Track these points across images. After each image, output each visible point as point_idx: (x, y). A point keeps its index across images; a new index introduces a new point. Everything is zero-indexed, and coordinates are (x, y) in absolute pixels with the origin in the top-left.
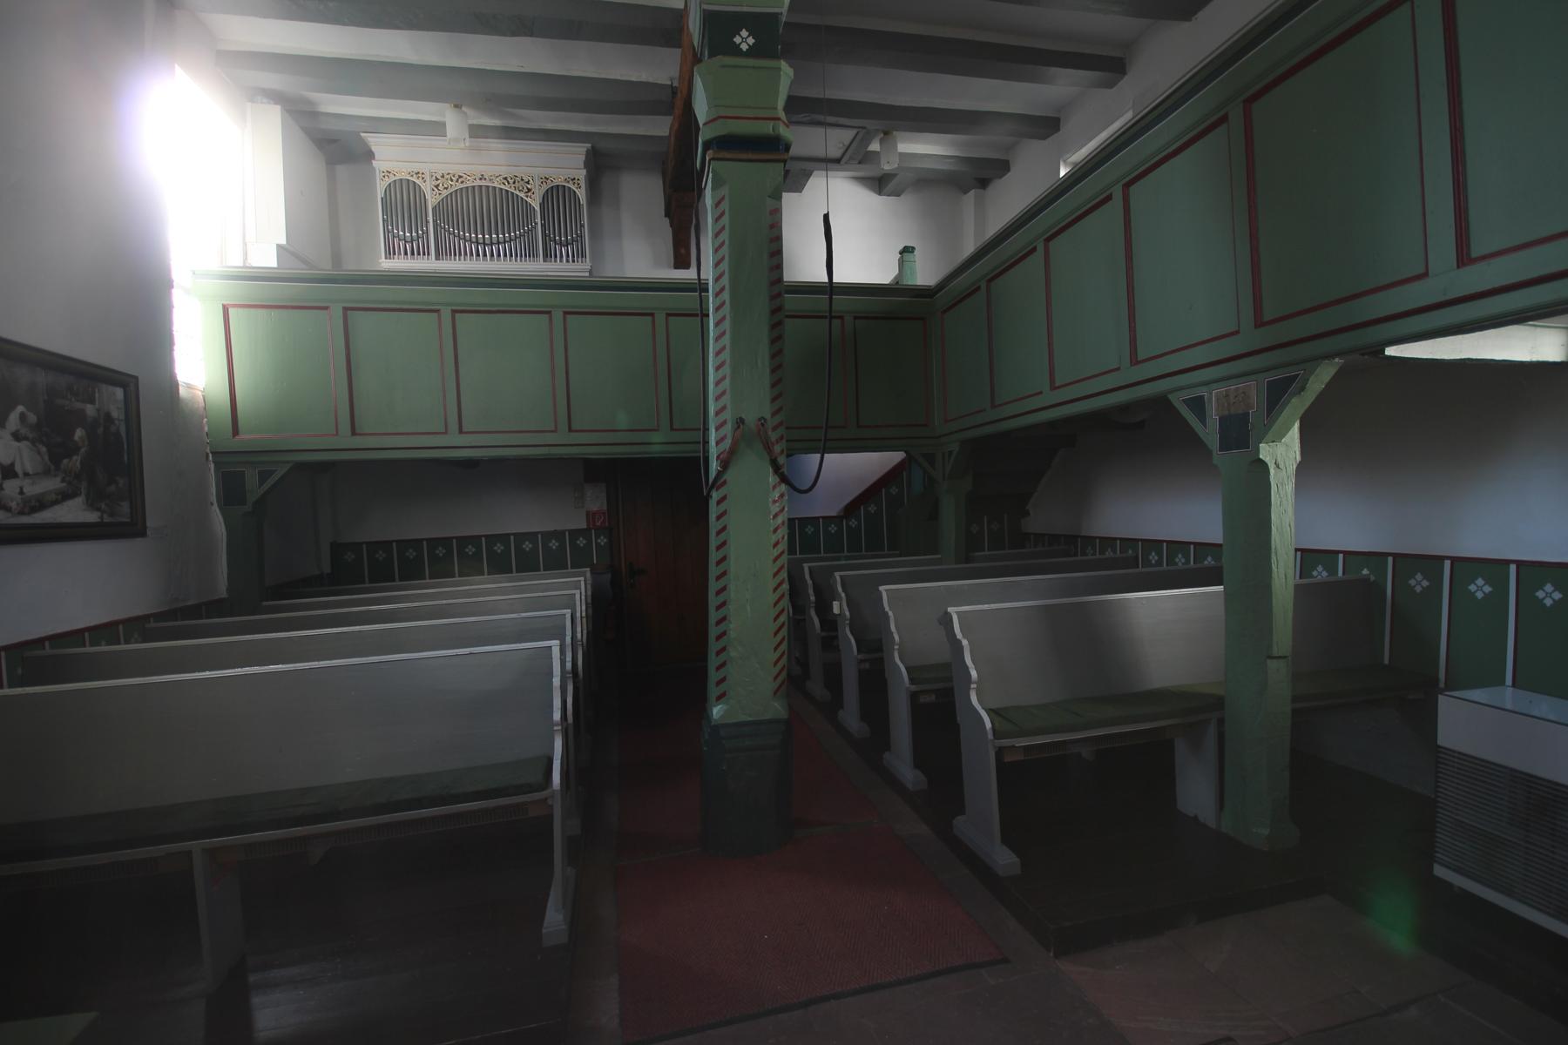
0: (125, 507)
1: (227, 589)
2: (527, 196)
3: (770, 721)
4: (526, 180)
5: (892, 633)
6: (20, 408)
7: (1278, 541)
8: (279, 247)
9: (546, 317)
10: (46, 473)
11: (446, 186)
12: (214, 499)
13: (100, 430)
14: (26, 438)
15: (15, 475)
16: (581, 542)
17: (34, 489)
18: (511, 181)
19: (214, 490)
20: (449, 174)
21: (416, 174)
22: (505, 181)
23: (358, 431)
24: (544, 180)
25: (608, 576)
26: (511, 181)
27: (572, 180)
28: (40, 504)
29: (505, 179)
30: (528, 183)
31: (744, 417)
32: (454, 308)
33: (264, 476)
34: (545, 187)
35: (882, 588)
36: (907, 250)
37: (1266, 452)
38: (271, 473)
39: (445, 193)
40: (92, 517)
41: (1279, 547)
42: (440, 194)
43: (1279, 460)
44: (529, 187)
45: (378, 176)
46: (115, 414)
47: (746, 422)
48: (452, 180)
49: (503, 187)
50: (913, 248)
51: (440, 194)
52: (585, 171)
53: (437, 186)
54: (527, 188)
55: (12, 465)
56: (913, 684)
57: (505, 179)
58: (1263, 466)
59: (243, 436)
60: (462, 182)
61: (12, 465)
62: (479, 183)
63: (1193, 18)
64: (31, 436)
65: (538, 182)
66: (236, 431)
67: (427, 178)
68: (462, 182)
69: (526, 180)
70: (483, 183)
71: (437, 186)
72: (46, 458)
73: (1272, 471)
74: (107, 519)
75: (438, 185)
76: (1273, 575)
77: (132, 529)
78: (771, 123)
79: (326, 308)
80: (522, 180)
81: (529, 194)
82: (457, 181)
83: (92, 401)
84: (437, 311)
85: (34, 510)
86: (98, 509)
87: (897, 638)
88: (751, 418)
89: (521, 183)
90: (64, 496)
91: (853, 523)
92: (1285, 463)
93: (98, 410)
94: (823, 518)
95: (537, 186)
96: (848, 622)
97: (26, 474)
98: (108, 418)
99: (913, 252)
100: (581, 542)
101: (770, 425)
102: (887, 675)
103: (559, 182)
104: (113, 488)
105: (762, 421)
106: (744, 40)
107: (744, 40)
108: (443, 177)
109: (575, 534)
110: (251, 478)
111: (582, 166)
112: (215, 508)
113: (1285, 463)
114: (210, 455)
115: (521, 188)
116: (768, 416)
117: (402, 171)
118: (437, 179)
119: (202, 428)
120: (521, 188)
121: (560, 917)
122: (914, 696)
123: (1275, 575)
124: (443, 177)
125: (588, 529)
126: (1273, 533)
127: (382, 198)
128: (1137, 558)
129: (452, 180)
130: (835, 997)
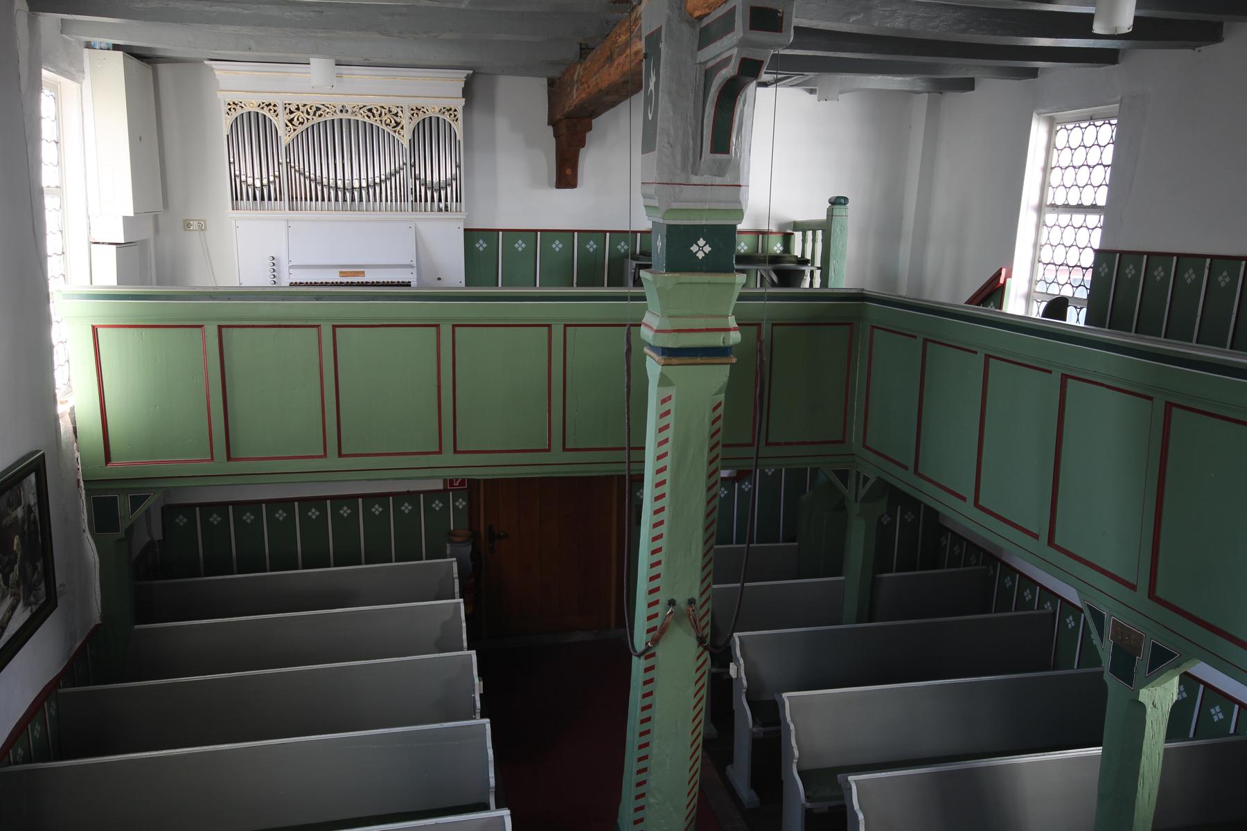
1: (101, 616)
2: (395, 131)
4: (394, 111)
5: (793, 748)
7: (1146, 768)
8: (126, 219)
11: (301, 120)
16: (437, 505)
19: (85, 516)
20: (305, 105)
21: (267, 106)
22: (370, 114)
23: (232, 456)
24: (416, 111)
25: (469, 548)
27: (448, 110)
29: (370, 110)
30: (396, 115)
31: (675, 598)
32: (335, 323)
33: (136, 502)
34: (416, 120)
35: (785, 695)
36: (837, 202)
37: (1145, 695)
39: (300, 128)
41: (373, 102)
42: (295, 130)
43: (1156, 702)
44: (398, 120)
47: (677, 603)
48: (308, 113)
49: (367, 119)
50: (846, 199)
51: (295, 130)
52: (464, 100)
54: (396, 122)
56: (808, 801)
57: (370, 110)
58: (1142, 707)
60: (321, 115)
62: (339, 116)
63: (1197, 49)
65: (408, 114)
66: (108, 458)
67: (280, 109)
68: (321, 115)
69: (394, 111)
70: (345, 116)
71: (291, 121)
73: (1149, 710)
75: (292, 119)
76: (1138, 795)
78: (723, 334)
80: (390, 111)
81: (398, 128)
82: (314, 115)
87: (796, 753)
88: (681, 600)
90: (13, 608)
91: (746, 486)
92: (1161, 704)
95: (407, 118)
96: (745, 690)
99: (845, 204)
100: (437, 505)
101: (698, 603)
102: (783, 778)
103: (433, 112)
105: (691, 602)
106: (701, 249)
107: (701, 249)
108: (298, 109)
109: (430, 495)
110: (124, 504)
111: (461, 96)
112: (88, 535)
113: (1161, 704)
114: (82, 484)
115: (388, 121)
116: (696, 595)
117: (251, 103)
118: (291, 112)
120: (388, 121)
122: (808, 813)
123: (1139, 795)
125: (445, 490)
126: (1142, 760)
127: (228, 136)
128: (1054, 614)
129: (308, 113)
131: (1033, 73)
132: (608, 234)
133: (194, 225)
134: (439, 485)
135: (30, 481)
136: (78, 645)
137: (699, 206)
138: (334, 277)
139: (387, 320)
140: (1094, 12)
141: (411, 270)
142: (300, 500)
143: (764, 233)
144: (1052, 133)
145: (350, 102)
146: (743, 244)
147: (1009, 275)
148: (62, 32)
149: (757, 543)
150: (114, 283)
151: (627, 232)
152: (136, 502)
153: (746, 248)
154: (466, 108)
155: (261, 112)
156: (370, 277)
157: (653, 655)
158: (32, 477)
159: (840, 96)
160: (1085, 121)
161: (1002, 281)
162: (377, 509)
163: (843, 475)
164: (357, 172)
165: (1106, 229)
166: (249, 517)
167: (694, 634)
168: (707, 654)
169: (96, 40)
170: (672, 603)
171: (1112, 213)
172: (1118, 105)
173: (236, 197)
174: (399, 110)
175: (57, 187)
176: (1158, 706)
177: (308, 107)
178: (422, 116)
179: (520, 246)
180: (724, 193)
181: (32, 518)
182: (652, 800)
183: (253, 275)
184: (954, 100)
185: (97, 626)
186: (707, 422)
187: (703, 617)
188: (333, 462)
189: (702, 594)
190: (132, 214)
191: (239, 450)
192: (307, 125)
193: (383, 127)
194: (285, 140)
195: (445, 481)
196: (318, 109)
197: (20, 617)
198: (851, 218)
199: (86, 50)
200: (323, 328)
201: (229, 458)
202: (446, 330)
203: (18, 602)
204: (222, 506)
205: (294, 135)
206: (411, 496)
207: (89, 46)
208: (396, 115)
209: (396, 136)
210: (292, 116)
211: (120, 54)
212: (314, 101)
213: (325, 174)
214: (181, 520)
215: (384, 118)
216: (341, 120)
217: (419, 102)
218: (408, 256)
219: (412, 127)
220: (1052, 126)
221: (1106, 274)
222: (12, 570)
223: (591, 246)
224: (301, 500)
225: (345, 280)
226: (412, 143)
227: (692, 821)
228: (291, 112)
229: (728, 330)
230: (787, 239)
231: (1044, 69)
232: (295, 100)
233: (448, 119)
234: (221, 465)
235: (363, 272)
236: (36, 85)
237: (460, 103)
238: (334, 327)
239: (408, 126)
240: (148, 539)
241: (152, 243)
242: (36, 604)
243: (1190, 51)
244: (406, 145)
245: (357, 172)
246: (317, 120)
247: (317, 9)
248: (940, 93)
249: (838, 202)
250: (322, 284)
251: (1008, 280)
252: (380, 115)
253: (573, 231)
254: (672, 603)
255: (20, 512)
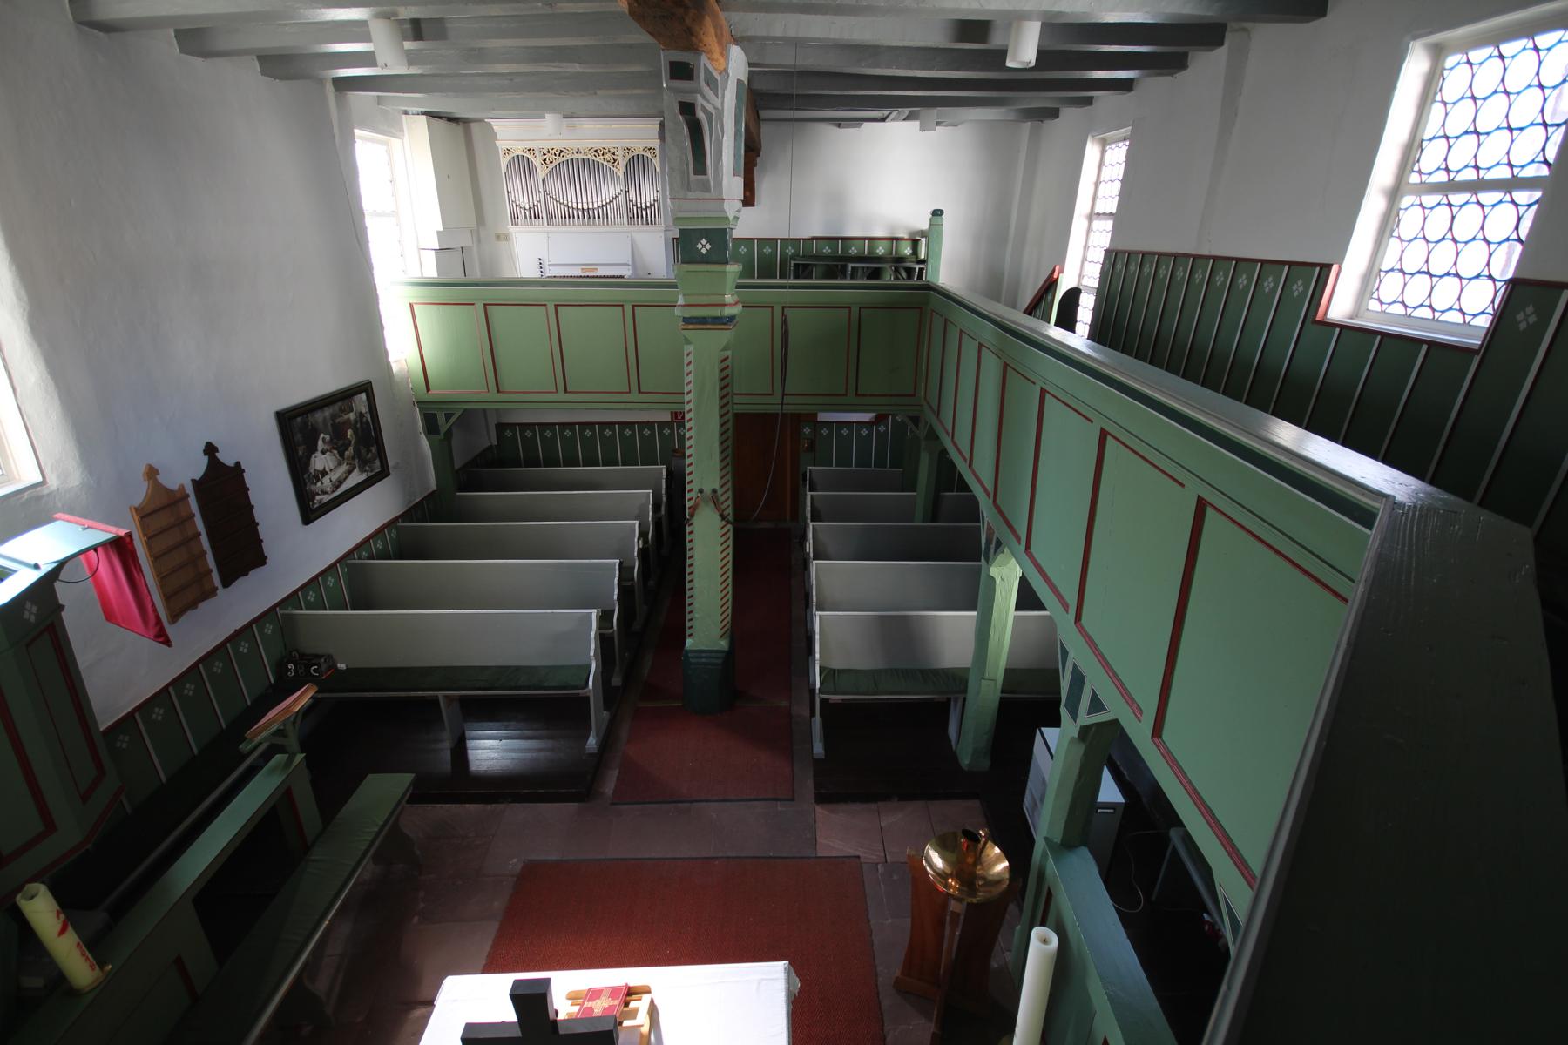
0: (377, 462)
3: (717, 651)
4: (612, 150)
6: (322, 435)
8: (438, 232)
9: (621, 307)
10: (340, 464)
12: (421, 430)
13: (358, 425)
14: (328, 451)
15: (327, 473)
16: (667, 431)
17: (335, 476)
18: (601, 153)
19: (420, 424)
21: (529, 150)
23: (501, 390)
26: (601, 153)
28: (340, 482)
29: (596, 151)
32: (557, 303)
33: (448, 416)
38: (452, 414)
40: (363, 477)
41: (598, 144)
44: (615, 157)
45: (501, 154)
46: (364, 411)
48: (555, 155)
53: (545, 161)
55: (324, 469)
57: (596, 151)
59: (433, 391)
61: (324, 469)
62: (576, 156)
64: (329, 448)
66: (428, 389)
67: (537, 152)
69: (612, 150)
71: (545, 161)
72: (337, 456)
74: (370, 474)
77: (384, 473)
79: (473, 304)
81: (616, 163)
83: (352, 411)
84: (545, 305)
85: (337, 487)
86: (365, 471)
88: (708, 490)
89: (609, 154)
90: (350, 472)
91: (882, 429)
93: (356, 414)
94: (857, 422)
97: (331, 470)
98: (361, 415)
100: (667, 431)
104: (370, 455)
107: (704, 246)
108: (548, 152)
109: (662, 425)
110: (441, 418)
112: (423, 435)
117: (518, 149)
118: (544, 154)
119: (408, 385)
121: (594, 742)
124: (548, 152)
129: (555, 155)
130: (707, 801)
131: (1089, 101)
132: (756, 241)
133: (502, 237)
134: (668, 418)
135: (361, 398)
136: (417, 500)
137: (696, 215)
138: (577, 272)
139: (581, 301)
140: (372, 49)
141: (627, 267)
142: (579, 424)
143: (897, 239)
144: (1103, 152)
145: (583, 145)
146: (880, 248)
147: (1062, 271)
148: (378, 104)
149: (890, 467)
150: (436, 275)
151: (787, 239)
152: (448, 416)
153: (883, 251)
154: (662, 148)
155: (525, 155)
156: (601, 272)
157: (692, 524)
158: (363, 396)
159: (937, 128)
160: (1121, 141)
161: (1055, 276)
162: (628, 432)
163: (915, 420)
164: (590, 198)
165: (1116, 232)
166: (548, 434)
167: (718, 514)
168: (729, 527)
169: (408, 109)
170: (701, 491)
171: (1120, 219)
172: (1130, 128)
173: (515, 217)
174: (615, 150)
175: (393, 212)
176: (1005, 579)
177: (554, 150)
178: (631, 155)
179: (704, 246)
180: (712, 205)
181: (364, 420)
182: (696, 615)
183: (525, 268)
184: (1050, 124)
185: (434, 492)
186: (717, 371)
187: (726, 500)
188: (561, 396)
189: (722, 486)
190: (442, 229)
191: (505, 386)
192: (555, 163)
193: (606, 163)
194: (541, 174)
195: (672, 413)
196: (562, 151)
197: (356, 478)
198: (948, 223)
199: (404, 116)
200: (548, 306)
201: (498, 391)
202: (628, 309)
203: (354, 469)
204: (531, 426)
205: (547, 171)
206: (649, 425)
207: (406, 113)
208: (614, 154)
209: (614, 169)
210: (545, 157)
211: (424, 117)
212: (558, 145)
213: (569, 200)
214: (508, 433)
215: (606, 156)
216: (578, 159)
217: (627, 143)
218: (627, 259)
219: (625, 163)
220: (1104, 144)
221: (1242, 277)
222: (347, 449)
223: (767, 250)
224: (560, 424)
225: (583, 274)
226: (625, 174)
227: (727, 631)
228: (544, 154)
229: (725, 305)
230: (915, 243)
231: (1097, 97)
232: (547, 145)
233: (650, 156)
234: (494, 396)
235: (597, 269)
236: (349, 141)
237: (656, 143)
238: (556, 306)
239: (623, 161)
240: (489, 444)
241: (475, 250)
242: (372, 471)
243: (1170, 78)
244: (622, 177)
245: (590, 198)
246: (561, 159)
247: (509, 78)
248: (1042, 121)
249: (937, 213)
250: (610, 277)
251: (1061, 275)
252: (603, 155)
253: (754, 239)
254: (701, 491)
255: (352, 416)
